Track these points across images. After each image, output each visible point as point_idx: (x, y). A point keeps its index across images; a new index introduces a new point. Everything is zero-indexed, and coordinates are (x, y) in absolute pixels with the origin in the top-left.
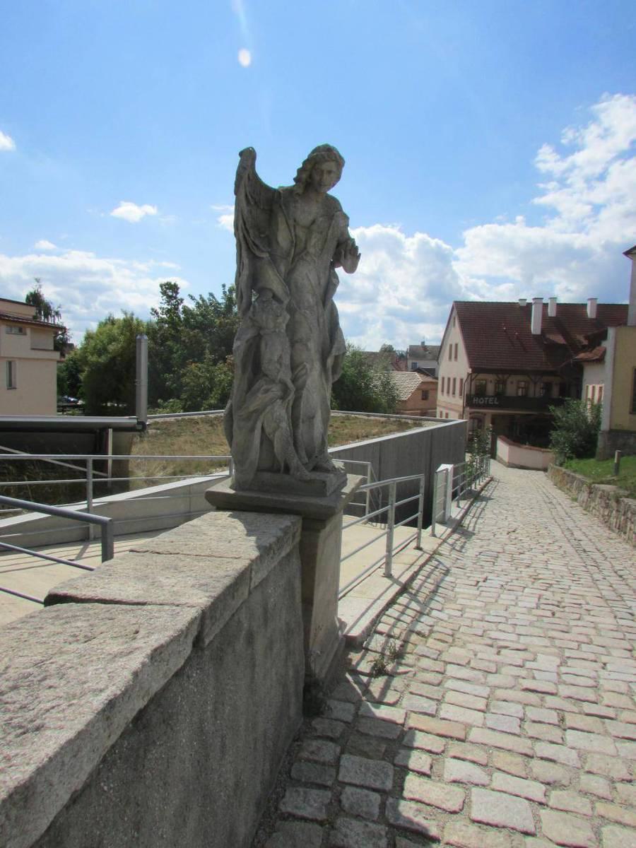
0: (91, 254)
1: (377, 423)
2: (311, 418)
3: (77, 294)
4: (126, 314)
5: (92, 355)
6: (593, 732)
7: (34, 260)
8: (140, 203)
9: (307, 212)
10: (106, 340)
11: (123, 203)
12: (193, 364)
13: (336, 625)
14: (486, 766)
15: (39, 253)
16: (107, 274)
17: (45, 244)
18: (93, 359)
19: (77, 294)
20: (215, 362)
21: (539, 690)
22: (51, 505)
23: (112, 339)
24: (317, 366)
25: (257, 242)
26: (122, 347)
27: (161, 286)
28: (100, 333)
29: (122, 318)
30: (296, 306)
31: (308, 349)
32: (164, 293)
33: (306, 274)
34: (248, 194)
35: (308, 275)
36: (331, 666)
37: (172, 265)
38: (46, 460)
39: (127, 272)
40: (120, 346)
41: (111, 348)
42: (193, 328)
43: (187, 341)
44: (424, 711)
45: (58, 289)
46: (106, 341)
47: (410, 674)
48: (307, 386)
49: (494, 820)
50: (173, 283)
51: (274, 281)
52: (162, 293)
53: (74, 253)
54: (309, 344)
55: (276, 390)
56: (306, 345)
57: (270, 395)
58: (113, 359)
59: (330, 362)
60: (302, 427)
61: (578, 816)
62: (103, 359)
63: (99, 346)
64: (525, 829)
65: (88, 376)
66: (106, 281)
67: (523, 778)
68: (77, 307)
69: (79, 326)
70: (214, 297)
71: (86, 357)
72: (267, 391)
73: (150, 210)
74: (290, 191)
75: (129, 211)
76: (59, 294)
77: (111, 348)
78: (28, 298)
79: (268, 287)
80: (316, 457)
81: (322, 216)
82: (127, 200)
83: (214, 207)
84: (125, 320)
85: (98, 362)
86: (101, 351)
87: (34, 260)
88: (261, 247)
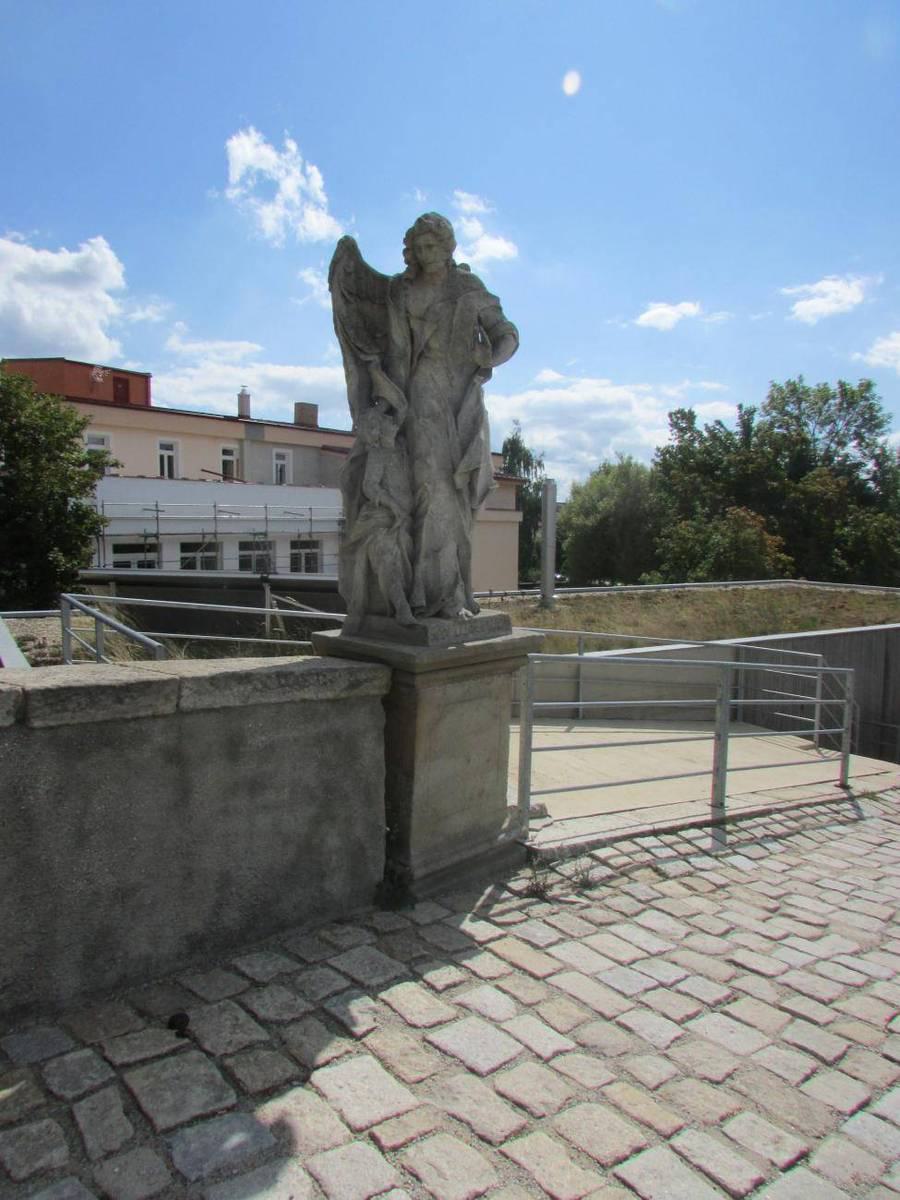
0: (605, 382)
1: (872, 601)
2: (435, 552)
3: (585, 437)
4: (621, 458)
5: (578, 515)
6: (755, 1027)
7: (536, 397)
8: (672, 301)
9: (419, 300)
10: (597, 495)
11: (652, 305)
12: (683, 522)
13: (502, 825)
14: (745, 1096)
15: (541, 387)
16: (626, 406)
17: (549, 375)
18: (577, 521)
19: (585, 437)
20: (709, 517)
21: (749, 966)
22: (137, 630)
23: (603, 494)
24: (443, 486)
25: (360, 346)
26: (616, 504)
27: (670, 415)
28: (590, 485)
29: (617, 465)
30: (413, 415)
31: (429, 467)
32: (674, 425)
33: (431, 375)
34: (346, 293)
35: (435, 379)
36: (442, 870)
37: (715, 386)
38: (338, 619)
39: (651, 401)
40: (613, 502)
41: (601, 505)
42: (691, 470)
43: (680, 490)
44: (526, 938)
45: (563, 432)
46: (596, 496)
47: (577, 906)
48: (429, 512)
49: (447, 1046)
50: (686, 411)
51: (389, 391)
52: (671, 425)
53: (585, 381)
54: (429, 461)
55: (380, 516)
56: (426, 462)
57: (372, 522)
58: (604, 522)
59: (460, 480)
60: (423, 564)
61: (573, 1083)
62: (590, 522)
63: (587, 505)
64: (473, 1066)
65: (571, 544)
66: (624, 416)
67: (559, 1032)
68: (584, 454)
69: (565, 475)
70: (722, 426)
71: (570, 519)
72: (368, 517)
73: (689, 308)
74: (399, 278)
75: (660, 315)
76: (561, 438)
77: (601, 505)
78: (505, 447)
79: (381, 395)
80: (443, 600)
81: (443, 300)
82: (658, 300)
83: (786, 291)
84: (621, 467)
85: (585, 526)
86: (587, 512)
87: (536, 397)
88: (366, 349)
